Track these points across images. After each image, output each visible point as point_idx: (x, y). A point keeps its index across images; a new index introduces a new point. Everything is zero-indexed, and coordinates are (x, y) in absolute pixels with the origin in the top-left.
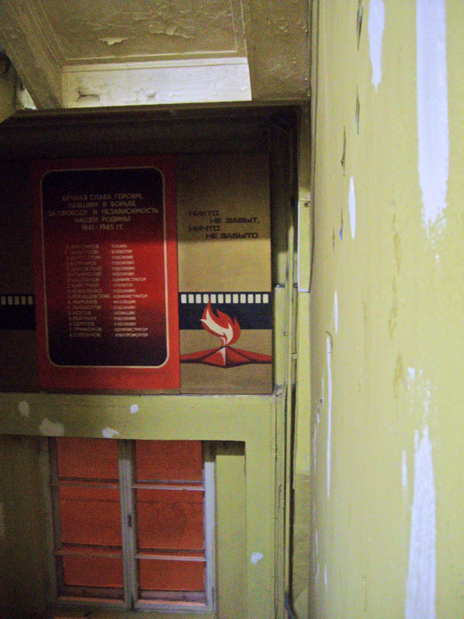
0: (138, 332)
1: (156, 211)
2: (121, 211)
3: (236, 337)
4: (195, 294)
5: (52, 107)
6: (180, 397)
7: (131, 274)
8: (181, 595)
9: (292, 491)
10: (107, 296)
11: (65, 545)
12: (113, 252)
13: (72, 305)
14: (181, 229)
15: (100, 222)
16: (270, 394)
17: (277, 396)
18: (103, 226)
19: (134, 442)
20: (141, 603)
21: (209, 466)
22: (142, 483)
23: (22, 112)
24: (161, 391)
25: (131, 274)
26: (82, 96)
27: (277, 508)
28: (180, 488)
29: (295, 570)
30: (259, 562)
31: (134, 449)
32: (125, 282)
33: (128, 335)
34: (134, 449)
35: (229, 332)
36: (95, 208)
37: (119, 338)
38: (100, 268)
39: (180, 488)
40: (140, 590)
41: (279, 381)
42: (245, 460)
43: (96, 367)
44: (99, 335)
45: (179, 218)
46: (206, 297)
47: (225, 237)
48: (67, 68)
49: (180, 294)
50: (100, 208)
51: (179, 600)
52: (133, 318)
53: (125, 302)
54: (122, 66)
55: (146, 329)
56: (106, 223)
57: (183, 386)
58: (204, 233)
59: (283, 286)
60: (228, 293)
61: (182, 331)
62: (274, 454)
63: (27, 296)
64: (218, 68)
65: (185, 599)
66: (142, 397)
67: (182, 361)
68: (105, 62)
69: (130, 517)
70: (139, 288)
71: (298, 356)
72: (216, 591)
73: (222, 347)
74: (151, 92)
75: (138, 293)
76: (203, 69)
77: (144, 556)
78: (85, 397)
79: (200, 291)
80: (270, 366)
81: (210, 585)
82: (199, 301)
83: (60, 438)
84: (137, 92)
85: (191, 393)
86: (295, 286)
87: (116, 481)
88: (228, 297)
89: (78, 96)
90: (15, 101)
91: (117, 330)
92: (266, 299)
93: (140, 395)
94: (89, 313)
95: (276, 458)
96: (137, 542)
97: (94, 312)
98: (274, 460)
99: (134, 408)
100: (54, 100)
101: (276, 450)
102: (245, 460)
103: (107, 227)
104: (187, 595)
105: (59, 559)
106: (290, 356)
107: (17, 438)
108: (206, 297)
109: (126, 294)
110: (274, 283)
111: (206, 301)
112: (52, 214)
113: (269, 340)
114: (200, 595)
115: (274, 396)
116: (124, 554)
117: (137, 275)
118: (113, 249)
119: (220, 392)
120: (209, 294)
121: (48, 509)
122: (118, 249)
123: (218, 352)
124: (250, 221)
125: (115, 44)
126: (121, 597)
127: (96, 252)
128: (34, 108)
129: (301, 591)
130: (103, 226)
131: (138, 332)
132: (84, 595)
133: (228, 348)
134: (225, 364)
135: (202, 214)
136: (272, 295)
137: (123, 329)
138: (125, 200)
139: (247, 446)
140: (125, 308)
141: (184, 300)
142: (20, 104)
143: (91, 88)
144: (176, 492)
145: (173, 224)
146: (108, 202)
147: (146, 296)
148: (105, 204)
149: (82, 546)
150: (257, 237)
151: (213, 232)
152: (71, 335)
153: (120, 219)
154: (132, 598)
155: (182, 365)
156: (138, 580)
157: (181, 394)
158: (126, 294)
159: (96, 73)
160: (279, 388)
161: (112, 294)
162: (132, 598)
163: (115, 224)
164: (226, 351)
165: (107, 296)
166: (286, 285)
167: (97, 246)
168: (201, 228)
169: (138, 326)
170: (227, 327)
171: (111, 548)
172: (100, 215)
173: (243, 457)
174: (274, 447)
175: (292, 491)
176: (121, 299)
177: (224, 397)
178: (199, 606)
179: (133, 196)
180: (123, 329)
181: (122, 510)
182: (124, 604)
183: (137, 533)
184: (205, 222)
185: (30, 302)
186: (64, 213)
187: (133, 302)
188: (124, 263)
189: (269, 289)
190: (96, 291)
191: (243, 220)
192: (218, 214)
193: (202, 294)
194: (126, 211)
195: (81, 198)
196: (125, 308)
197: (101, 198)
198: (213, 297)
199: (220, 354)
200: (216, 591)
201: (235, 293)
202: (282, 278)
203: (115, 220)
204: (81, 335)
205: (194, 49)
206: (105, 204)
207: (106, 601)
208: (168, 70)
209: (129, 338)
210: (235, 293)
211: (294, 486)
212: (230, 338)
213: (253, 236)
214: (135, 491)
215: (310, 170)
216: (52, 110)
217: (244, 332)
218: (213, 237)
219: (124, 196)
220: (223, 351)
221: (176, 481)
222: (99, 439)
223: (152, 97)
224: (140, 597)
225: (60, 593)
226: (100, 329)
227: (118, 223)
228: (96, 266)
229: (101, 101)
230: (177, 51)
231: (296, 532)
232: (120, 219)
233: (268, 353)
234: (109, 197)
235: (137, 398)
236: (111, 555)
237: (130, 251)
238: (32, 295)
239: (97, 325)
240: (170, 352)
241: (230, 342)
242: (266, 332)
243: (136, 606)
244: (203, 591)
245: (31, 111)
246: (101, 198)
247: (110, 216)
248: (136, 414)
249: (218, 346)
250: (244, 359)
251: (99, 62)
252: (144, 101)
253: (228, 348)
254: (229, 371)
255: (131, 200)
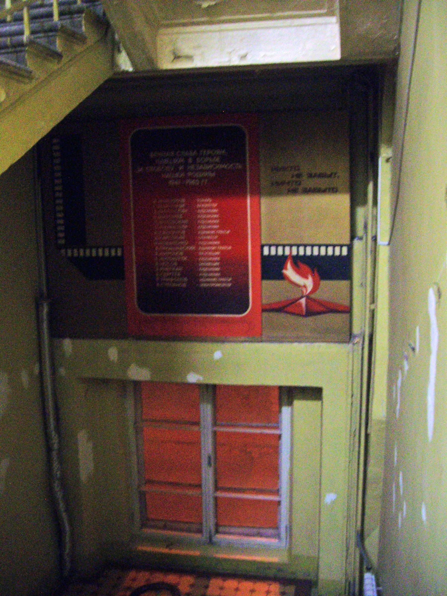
0: (222, 282)
1: (240, 167)
2: (207, 167)
3: (316, 287)
4: (277, 246)
5: (148, 68)
6: (260, 344)
7: (215, 227)
8: (255, 531)
9: (367, 436)
10: (192, 248)
11: (149, 482)
12: (199, 206)
13: (159, 257)
14: (264, 182)
15: (186, 178)
16: (348, 342)
17: (354, 344)
18: (188, 181)
19: (215, 387)
20: (219, 537)
21: (286, 411)
22: (222, 426)
23: (118, 73)
24: (243, 338)
25: (215, 227)
26: (177, 57)
27: (351, 450)
28: (258, 431)
29: (367, 511)
30: (333, 502)
31: (214, 394)
32: (209, 235)
33: (213, 285)
34: (214, 394)
35: (309, 283)
36: (181, 164)
37: (205, 289)
38: (186, 221)
39: (258, 431)
40: (217, 525)
41: (356, 330)
42: (322, 405)
43: (175, 315)
44: (184, 285)
45: (262, 175)
46: (287, 249)
47: (308, 191)
48: (162, 31)
49: (262, 247)
50: (186, 164)
51: (253, 535)
52: (218, 269)
53: (210, 253)
54: (215, 27)
55: (230, 279)
56: (192, 178)
57: (264, 333)
58: (285, 187)
59: (361, 239)
60: (274, 245)
61: (265, 282)
62: (350, 400)
63: (116, 248)
64: (307, 28)
65: (260, 535)
66: (226, 343)
67: (265, 310)
68: (198, 24)
69: (209, 458)
70: (223, 239)
71: (376, 306)
72: (290, 529)
73: (302, 297)
74: (243, 52)
75: (222, 244)
76: (293, 29)
77: (220, 494)
78: (173, 344)
79: (317, 242)
80: (348, 315)
81: (284, 523)
82: (280, 252)
83: (146, 382)
84: (230, 53)
85: (271, 340)
86: (375, 239)
87: (197, 423)
88: (309, 249)
89: (172, 57)
90: (113, 63)
91: (201, 280)
92: (345, 251)
93: (223, 342)
94: (176, 264)
95: (352, 404)
96: (216, 482)
97: (180, 263)
98: (349, 406)
99: (217, 355)
100: (151, 61)
101: (352, 396)
102: (322, 405)
103: (193, 182)
104: (262, 531)
105: (142, 495)
106: (368, 305)
107: (105, 382)
108: (287, 249)
109: (211, 245)
110: (353, 236)
111: (287, 252)
112: (140, 170)
113: (346, 291)
114: (270, 531)
115: (351, 345)
116: (204, 491)
117: (221, 228)
118: (199, 203)
119: (299, 340)
120: (291, 246)
121: (133, 448)
122: (203, 203)
123: (298, 302)
124: (330, 176)
125: (209, 7)
126: (200, 531)
127: (183, 206)
128: (131, 69)
129: (373, 529)
130: (188, 181)
131: (222, 282)
132: (165, 527)
133: (308, 297)
134: (304, 313)
135: (284, 169)
136: (350, 248)
137: (208, 280)
138: (210, 156)
139: (325, 393)
140: (210, 259)
141: (266, 251)
142: (117, 66)
143: (185, 49)
144: (251, 435)
145: (256, 179)
146: (194, 158)
147: (230, 248)
148: (190, 160)
149: (160, 483)
150: (336, 191)
151: (294, 186)
152: (158, 285)
153: (206, 174)
154: (210, 532)
155: (265, 314)
156: (216, 515)
157: (261, 341)
158: (211, 245)
159: (190, 36)
160: (355, 337)
161: (198, 246)
162: (210, 532)
163: (200, 179)
164: (307, 302)
165: (192, 248)
166: (364, 238)
167: (183, 200)
168: (283, 183)
169: (222, 276)
170: (307, 278)
171: (191, 486)
172: (186, 170)
173: (319, 403)
174: (350, 392)
175: (367, 436)
176: (206, 251)
177: (303, 345)
178: (274, 542)
179: (218, 152)
180: (208, 280)
181: (203, 451)
182: (204, 537)
183: (216, 473)
184: (287, 176)
185: (119, 254)
186: (152, 169)
187: (218, 253)
188: (209, 216)
189: (347, 241)
190: (182, 243)
191: (321, 176)
192: (299, 170)
193: (305, 246)
194: (211, 166)
195: (168, 154)
196: (210, 259)
197: (186, 154)
198: (294, 249)
199: (300, 305)
200: (290, 529)
201: (280, 245)
202: (360, 231)
203: (201, 175)
204: (167, 284)
205: (283, 10)
206: (190, 160)
207: (184, 534)
208: (259, 32)
209: (214, 288)
210: (280, 245)
211: (369, 431)
212: (310, 288)
213: (334, 190)
214: (215, 433)
215: (392, 126)
216: (149, 71)
217: (324, 283)
218: (294, 192)
219: (209, 152)
220: (303, 301)
221: (254, 424)
222: (177, 384)
223: (244, 57)
224: (217, 532)
225: (143, 525)
226: (186, 279)
227: (205, 178)
228: (184, 219)
229: (195, 62)
230: (267, 11)
231: (369, 475)
232: (206, 174)
233: (347, 303)
234: (195, 153)
235: (220, 345)
236: (190, 492)
237: (215, 205)
238: (122, 247)
239: (183, 275)
240: (253, 302)
241: (310, 292)
242: (344, 283)
243: (214, 539)
244: (277, 527)
245: (127, 72)
246: (186, 154)
247: (196, 171)
248: (217, 361)
249: (298, 296)
250: (322, 309)
251: (193, 24)
252: (236, 61)
253: (308, 297)
254: (309, 320)
255: (217, 156)
